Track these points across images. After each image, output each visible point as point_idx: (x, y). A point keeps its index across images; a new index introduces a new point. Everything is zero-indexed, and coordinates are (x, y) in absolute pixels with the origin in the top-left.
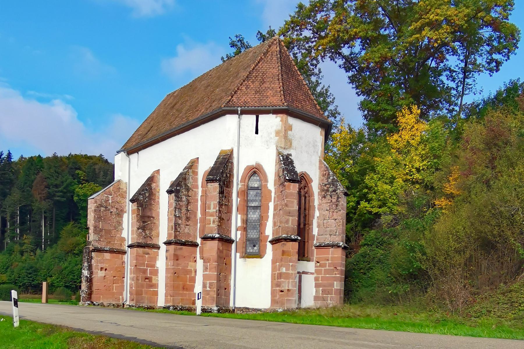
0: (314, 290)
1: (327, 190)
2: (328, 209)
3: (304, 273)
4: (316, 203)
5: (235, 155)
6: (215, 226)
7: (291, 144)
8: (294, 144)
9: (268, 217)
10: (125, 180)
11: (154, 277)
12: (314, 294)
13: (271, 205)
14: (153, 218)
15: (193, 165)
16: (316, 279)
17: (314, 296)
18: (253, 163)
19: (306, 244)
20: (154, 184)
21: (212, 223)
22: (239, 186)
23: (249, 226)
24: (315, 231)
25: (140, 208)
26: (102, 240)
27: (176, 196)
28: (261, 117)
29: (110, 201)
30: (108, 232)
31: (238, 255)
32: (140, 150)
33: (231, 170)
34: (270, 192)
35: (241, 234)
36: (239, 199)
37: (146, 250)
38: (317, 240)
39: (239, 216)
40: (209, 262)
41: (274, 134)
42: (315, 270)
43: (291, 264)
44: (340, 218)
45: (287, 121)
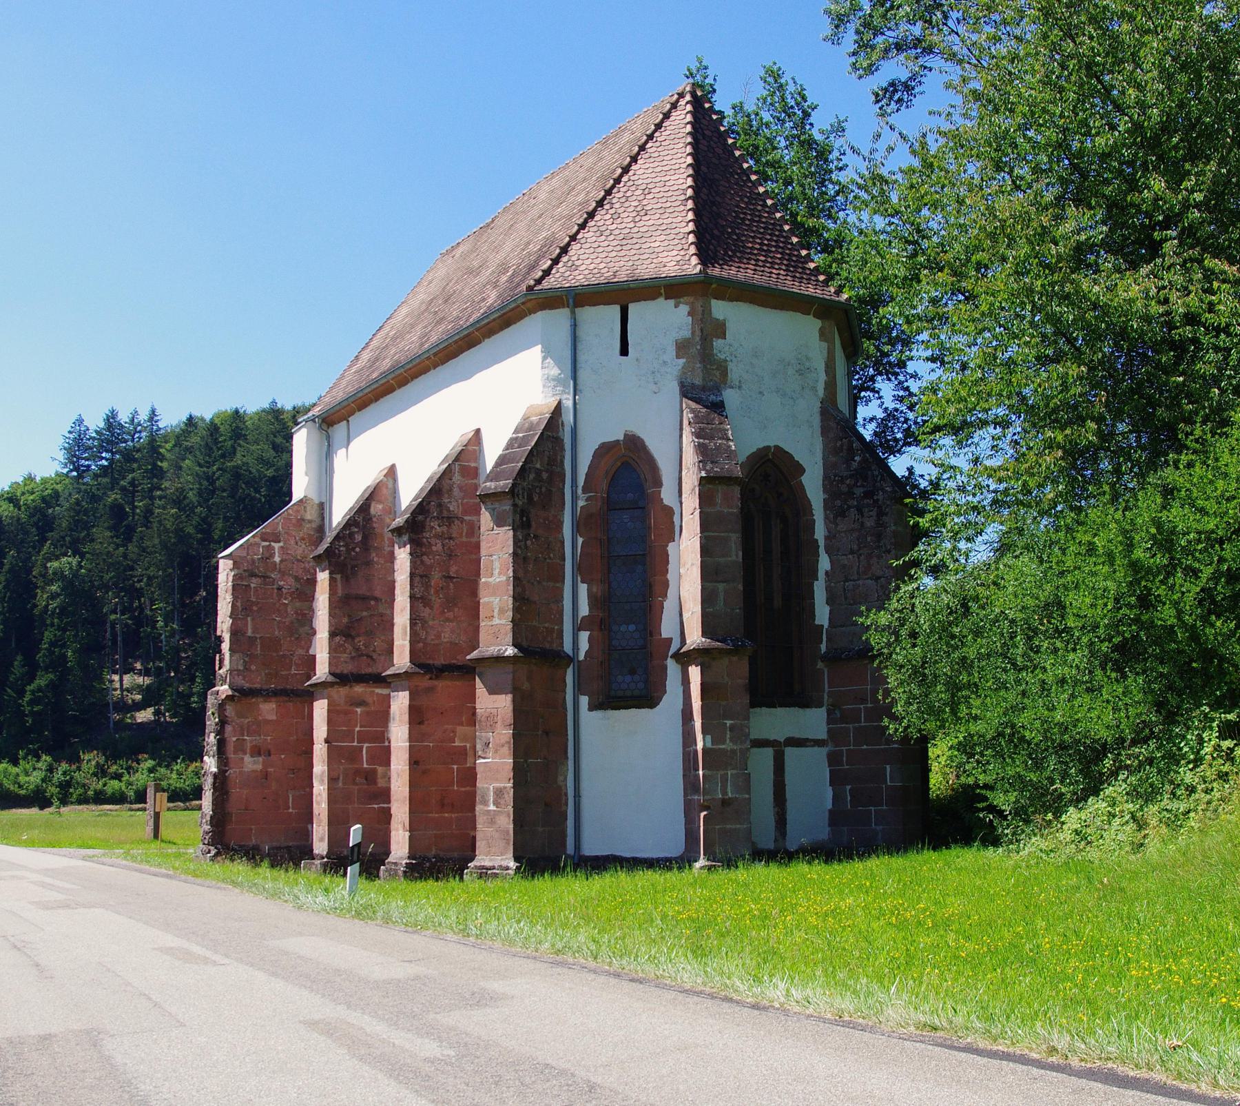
0: (829, 793)
1: (850, 494)
2: (855, 547)
4: (820, 533)
5: (568, 418)
7: (725, 373)
11: (380, 770)
12: (829, 806)
14: (376, 599)
16: (833, 759)
17: (830, 811)
21: (496, 614)
22: (581, 503)
25: (338, 577)
28: (633, 309)
29: (277, 559)
31: (584, 700)
32: (352, 413)
35: (590, 640)
36: (580, 540)
37: (359, 689)
38: (829, 639)
39: (583, 589)
41: (672, 351)
42: (829, 731)
45: (707, 310)
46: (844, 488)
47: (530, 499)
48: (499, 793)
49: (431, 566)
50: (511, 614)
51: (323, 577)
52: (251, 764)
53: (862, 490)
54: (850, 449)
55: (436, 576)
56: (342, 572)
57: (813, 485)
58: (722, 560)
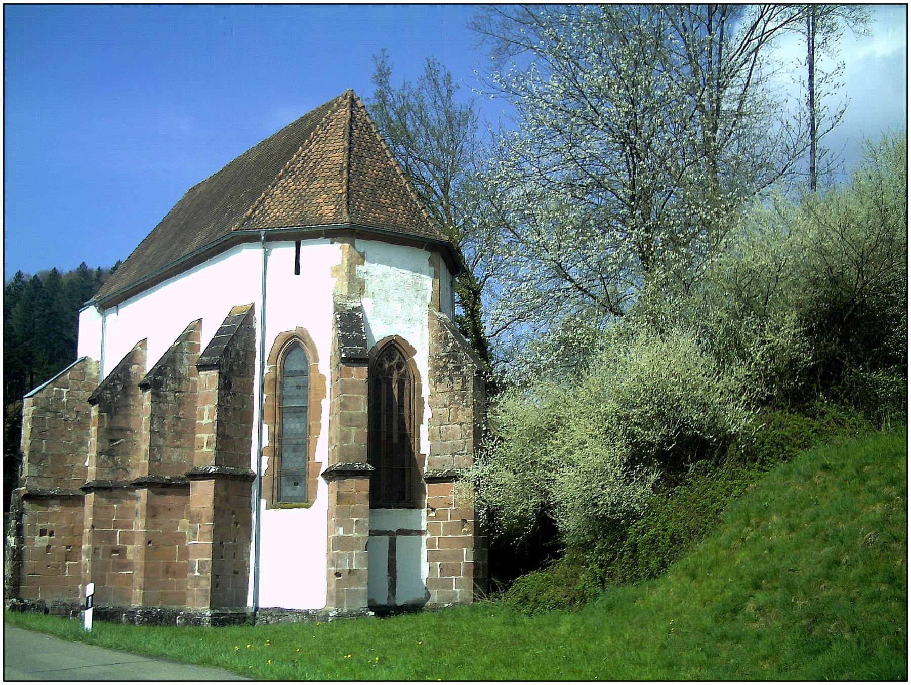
1: (446, 367)
2: (448, 403)
3: (402, 532)
4: (426, 393)
6: (210, 450)
8: (370, 287)
9: (320, 426)
10: (95, 357)
13: (326, 404)
14: (131, 430)
15: (189, 335)
18: (289, 327)
19: (407, 474)
20: (135, 367)
23: (285, 447)
24: (425, 447)
25: (105, 414)
26: (45, 475)
27: (153, 393)
30: (59, 459)
31: (263, 502)
33: (250, 343)
34: (323, 378)
40: (199, 521)
43: (355, 519)
44: (469, 420)
46: (442, 364)
47: (231, 369)
48: (202, 564)
49: (167, 410)
50: (214, 445)
51: (94, 411)
52: (41, 542)
53: (453, 365)
54: (446, 338)
55: (169, 420)
56: (109, 412)
57: (422, 362)
58: (354, 412)
